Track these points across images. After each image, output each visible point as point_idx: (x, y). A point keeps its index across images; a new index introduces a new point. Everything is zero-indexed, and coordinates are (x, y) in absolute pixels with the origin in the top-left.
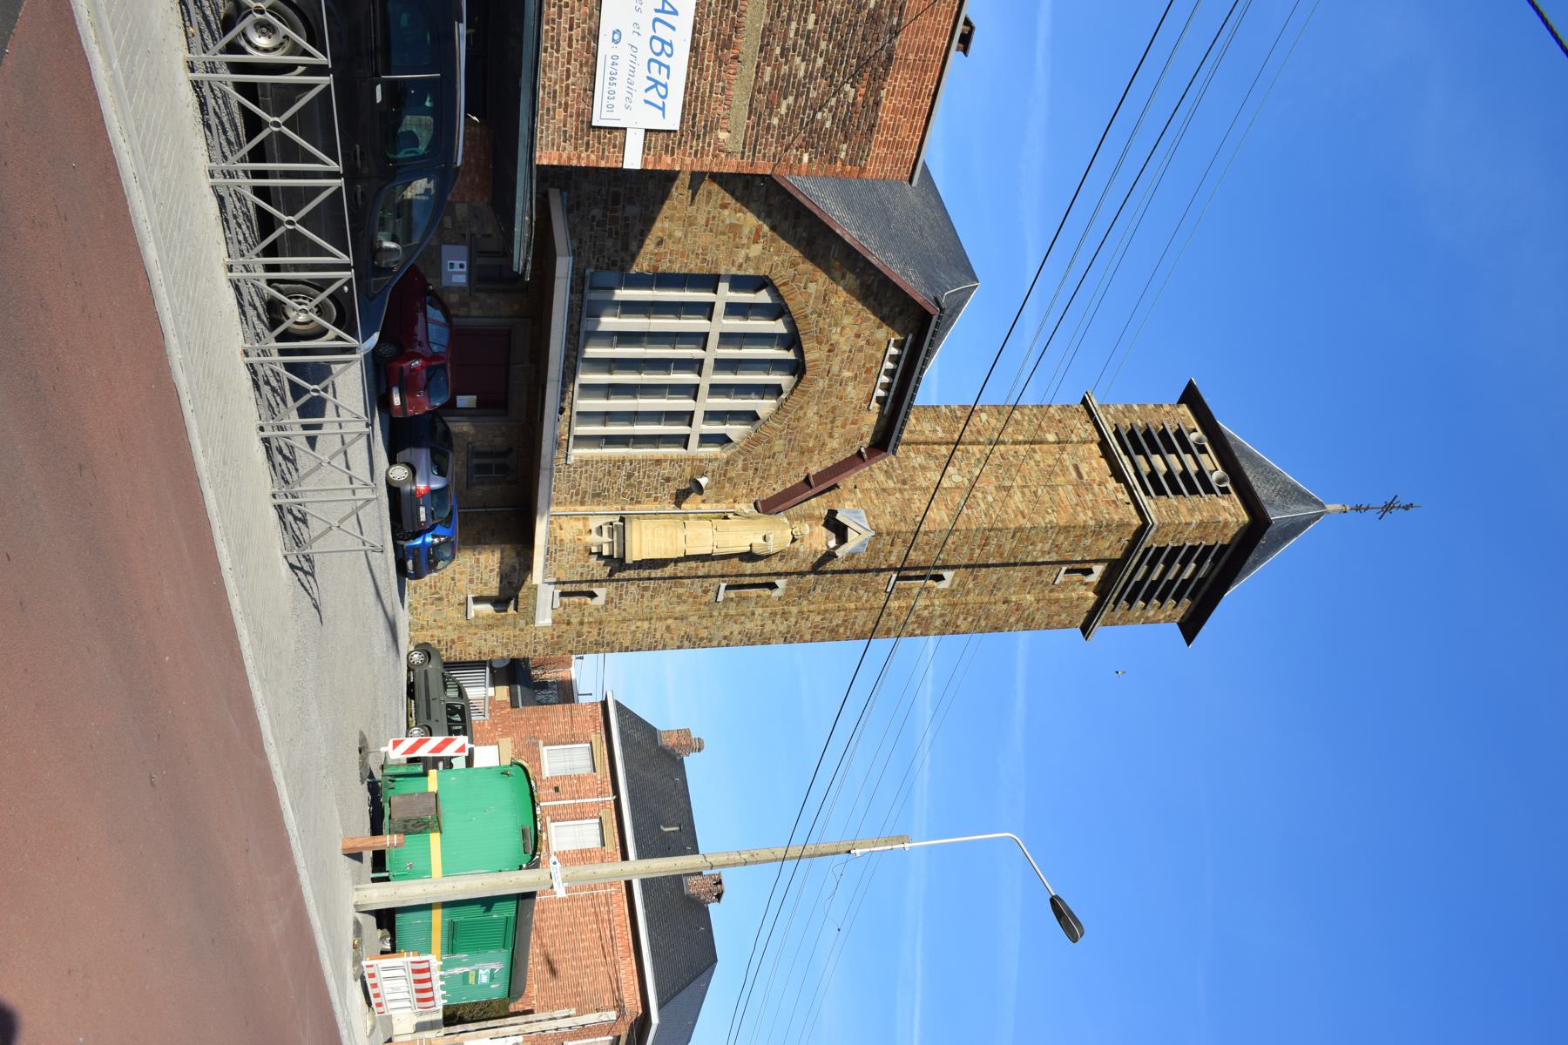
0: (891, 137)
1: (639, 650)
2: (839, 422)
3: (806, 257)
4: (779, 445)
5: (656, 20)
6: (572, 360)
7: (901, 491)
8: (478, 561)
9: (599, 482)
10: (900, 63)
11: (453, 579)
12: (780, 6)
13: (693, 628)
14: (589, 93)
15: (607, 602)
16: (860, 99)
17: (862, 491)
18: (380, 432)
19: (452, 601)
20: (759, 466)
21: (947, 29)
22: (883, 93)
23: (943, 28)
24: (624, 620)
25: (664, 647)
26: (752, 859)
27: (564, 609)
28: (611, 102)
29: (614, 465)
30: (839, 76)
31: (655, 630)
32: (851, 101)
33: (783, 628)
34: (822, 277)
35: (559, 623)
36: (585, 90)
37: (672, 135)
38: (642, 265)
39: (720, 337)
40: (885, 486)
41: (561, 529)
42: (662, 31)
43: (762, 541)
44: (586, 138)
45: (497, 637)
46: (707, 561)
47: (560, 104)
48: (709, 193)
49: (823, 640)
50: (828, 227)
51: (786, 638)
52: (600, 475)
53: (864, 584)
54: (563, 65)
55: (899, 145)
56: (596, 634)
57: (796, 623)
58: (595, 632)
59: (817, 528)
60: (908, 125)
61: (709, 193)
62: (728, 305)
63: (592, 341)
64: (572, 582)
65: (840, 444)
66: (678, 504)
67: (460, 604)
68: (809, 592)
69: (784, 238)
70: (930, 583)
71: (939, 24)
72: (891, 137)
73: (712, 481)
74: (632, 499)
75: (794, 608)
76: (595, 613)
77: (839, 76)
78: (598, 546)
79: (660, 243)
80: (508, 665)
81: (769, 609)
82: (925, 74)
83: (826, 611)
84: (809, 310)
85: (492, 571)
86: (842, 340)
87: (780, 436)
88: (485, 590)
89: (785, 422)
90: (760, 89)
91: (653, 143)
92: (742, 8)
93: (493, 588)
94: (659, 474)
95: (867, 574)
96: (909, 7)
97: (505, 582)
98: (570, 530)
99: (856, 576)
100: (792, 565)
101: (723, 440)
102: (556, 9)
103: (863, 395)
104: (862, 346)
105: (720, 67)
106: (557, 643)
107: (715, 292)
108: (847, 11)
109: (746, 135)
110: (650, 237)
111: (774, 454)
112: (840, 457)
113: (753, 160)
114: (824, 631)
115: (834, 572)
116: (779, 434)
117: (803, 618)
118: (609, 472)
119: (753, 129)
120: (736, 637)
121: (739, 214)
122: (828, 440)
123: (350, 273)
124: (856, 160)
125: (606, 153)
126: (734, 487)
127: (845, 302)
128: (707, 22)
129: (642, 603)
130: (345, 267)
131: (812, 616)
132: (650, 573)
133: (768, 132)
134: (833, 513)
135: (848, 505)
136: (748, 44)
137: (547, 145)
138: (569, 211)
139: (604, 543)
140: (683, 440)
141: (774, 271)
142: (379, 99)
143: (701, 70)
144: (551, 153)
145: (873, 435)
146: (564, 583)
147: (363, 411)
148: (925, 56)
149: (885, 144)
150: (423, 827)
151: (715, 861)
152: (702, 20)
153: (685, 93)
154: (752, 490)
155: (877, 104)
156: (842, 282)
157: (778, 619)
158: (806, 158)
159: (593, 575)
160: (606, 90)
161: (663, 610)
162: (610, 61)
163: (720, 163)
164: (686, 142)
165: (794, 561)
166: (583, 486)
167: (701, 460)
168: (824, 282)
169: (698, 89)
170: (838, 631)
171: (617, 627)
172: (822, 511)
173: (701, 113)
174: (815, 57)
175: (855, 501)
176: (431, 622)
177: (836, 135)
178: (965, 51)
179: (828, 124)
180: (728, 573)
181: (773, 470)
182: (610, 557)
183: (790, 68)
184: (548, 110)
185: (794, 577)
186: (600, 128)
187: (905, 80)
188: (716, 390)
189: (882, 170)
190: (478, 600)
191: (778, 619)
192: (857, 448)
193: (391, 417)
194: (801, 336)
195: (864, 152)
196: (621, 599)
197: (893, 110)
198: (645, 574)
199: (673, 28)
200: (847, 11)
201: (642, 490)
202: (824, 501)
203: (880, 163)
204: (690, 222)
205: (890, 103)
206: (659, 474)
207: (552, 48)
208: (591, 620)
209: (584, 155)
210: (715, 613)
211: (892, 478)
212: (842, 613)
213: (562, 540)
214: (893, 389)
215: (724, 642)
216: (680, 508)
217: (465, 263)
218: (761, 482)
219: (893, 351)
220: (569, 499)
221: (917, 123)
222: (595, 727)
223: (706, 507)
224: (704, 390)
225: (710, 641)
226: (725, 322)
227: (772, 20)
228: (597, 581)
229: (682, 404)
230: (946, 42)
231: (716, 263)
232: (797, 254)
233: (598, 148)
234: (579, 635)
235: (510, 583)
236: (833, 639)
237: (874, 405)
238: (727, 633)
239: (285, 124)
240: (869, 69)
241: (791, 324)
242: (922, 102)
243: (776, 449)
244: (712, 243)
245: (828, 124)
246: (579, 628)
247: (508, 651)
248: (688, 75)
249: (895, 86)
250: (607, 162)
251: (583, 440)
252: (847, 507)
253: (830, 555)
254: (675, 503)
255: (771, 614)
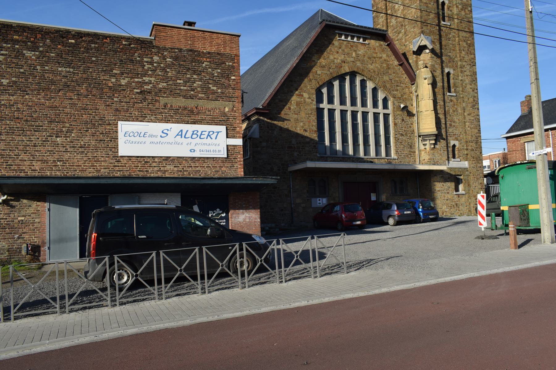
0: (222, 46)
1: (479, 125)
2: (375, 55)
3: (307, 76)
4: (386, 78)
5: (185, 137)
6: (354, 159)
7: (405, 26)
8: (439, 191)
9: (405, 146)
10: (192, 46)
11: (447, 200)
12: (175, 93)
13: (469, 104)
14: (215, 159)
15: (457, 140)
16: (208, 60)
17: (406, 42)
18: (373, 229)
19: (457, 200)
20: (395, 85)
21: (178, 30)
22: (205, 51)
23: (177, 32)
24: (465, 133)
25: (478, 115)
26: (533, 60)
27: (461, 156)
28: (217, 151)
29: (398, 141)
30: (200, 69)
31: (470, 120)
32: (209, 63)
33: (468, 67)
34: (314, 69)
35: (467, 158)
36: (214, 160)
37: (228, 128)
38: (315, 136)
39: (342, 105)
40: (404, 33)
41: (425, 160)
42: (189, 135)
43: (426, 80)
44: (232, 159)
45: (474, 182)
46: (437, 101)
47: (220, 169)
48: (285, 114)
49: (474, 50)
50: (293, 69)
51: (473, 65)
52: (402, 146)
53: (446, 35)
54: (205, 169)
55: (225, 42)
56: (472, 143)
57: (465, 62)
58: (471, 144)
59: (421, 58)
60: (216, 40)
61: (285, 114)
62: (329, 103)
63: (347, 153)
64: (448, 154)
65: (384, 54)
66: (414, 115)
67: (459, 197)
68: (451, 58)
69: (301, 85)
70: (446, 7)
71: (176, 34)
72: (222, 46)
73: (402, 103)
74: (412, 133)
75: (459, 64)
76: (462, 144)
77: (200, 69)
78: (431, 145)
79: (306, 131)
80: (491, 177)
81: (460, 74)
82: (196, 36)
83: (459, 50)
84: (328, 73)
85: (443, 185)
86: (340, 58)
87: (382, 78)
88: (452, 188)
89: (376, 77)
90: (207, 98)
91: (232, 135)
92: (178, 107)
93: (452, 185)
94: (401, 124)
95: (442, 34)
96: (171, 46)
97: (448, 180)
98: (425, 156)
99: (443, 39)
100: (438, 67)
101: (385, 101)
102: (185, 172)
103: (362, 47)
104: (342, 50)
105: (201, 113)
106: (477, 158)
107: (324, 109)
108: (175, 69)
109: (226, 101)
110: (303, 134)
111: (390, 79)
112: (390, 53)
113: (235, 97)
114: (470, 50)
115: (441, 48)
116: (381, 79)
117: (463, 59)
118: (400, 143)
119: (223, 99)
120: (473, 86)
121: (292, 103)
122: (383, 59)
123: (315, 237)
124: (232, 58)
125: (237, 151)
126: (405, 94)
127: (324, 59)
128: (184, 119)
129: (457, 126)
130: (158, 255)
131: (462, 55)
132: (443, 124)
133: (224, 93)
134: (414, 53)
135: (411, 47)
136: (191, 104)
137: (236, 173)
138: (295, 163)
139: (429, 143)
140: (386, 116)
141: (313, 88)
142: (145, 237)
143: (202, 120)
144: (239, 171)
145: (380, 41)
146: (448, 157)
147: (336, 237)
148: (188, 37)
149: (224, 48)
150: (525, 212)
151: (534, 78)
152: (184, 121)
153: (212, 125)
154: (406, 87)
155: (209, 53)
156: (316, 61)
157: (464, 69)
158: (233, 78)
159: (444, 146)
160: (216, 153)
161: (460, 117)
162: (202, 153)
163: (238, 109)
164: (231, 123)
165: (436, 66)
166: (407, 152)
167: (394, 108)
168: (317, 68)
169: (209, 120)
170: (469, 44)
171: (469, 135)
172: (414, 57)
173: (219, 118)
174: (193, 78)
175: (410, 44)
176: (467, 208)
177: (223, 67)
178: (195, 23)
179: (219, 71)
180: (442, 92)
181: (397, 79)
182: (435, 140)
183: (198, 87)
184: (222, 173)
185: (444, 65)
186: (227, 154)
187: (199, 44)
188: (364, 104)
189: (235, 48)
190: (457, 190)
191: (464, 69)
192: (386, 47)
193: (366, 224)
194: (339, 74)
195: (229, 56)
196: (456, 135)
197: (211, 47)
198: (443, 126)
199: (187, 131)
200: (175, 69)
201: (408, 130)
202: (410, 57)
203: (233, 49)
204: (297, 120)
205: (208, 48)
206: (401, 124)
207: (199, 173)
208: (465, 146)
209: (239, 160)
210: (462, 96)
211: (401, 31)
212: (461, 43)
213: (429, 159)
214: (359, 35)
215: (476, 91)
216: (415, 114)
217: (318, 199)
218: (403, 84)
219: (343, 38)
220: (413, 157)
221: (215, 37)
222: (517, 141)
223: (415, 104)
224: (364, 109)
225: (475, 97)
226: (336, 104)
227: (181, 96)
228: (447, 145)
229: (371, 118)
230: (182, 30)
231: (312, 109)
232: (306, 80)
233: (235, 155)
234: (473, 150)
235: (449, 178)
236: (474, 45)
237: (367, 42)
238: (471, 90)
239: (261, 258)
240: (196, 58)
241: (335, 79)
242: (207, 36)
243: (388, 79)
244: (304, 111)
245: (219, 71)
246: (469, 150)
247: (481, 178)
248: (204, 124)
249: (201, 47)
250: (241, 151)
251: (388, 153)
252: (412, 47)
253: (433, 51)
254: (413, 116)
255: (461, 73)
